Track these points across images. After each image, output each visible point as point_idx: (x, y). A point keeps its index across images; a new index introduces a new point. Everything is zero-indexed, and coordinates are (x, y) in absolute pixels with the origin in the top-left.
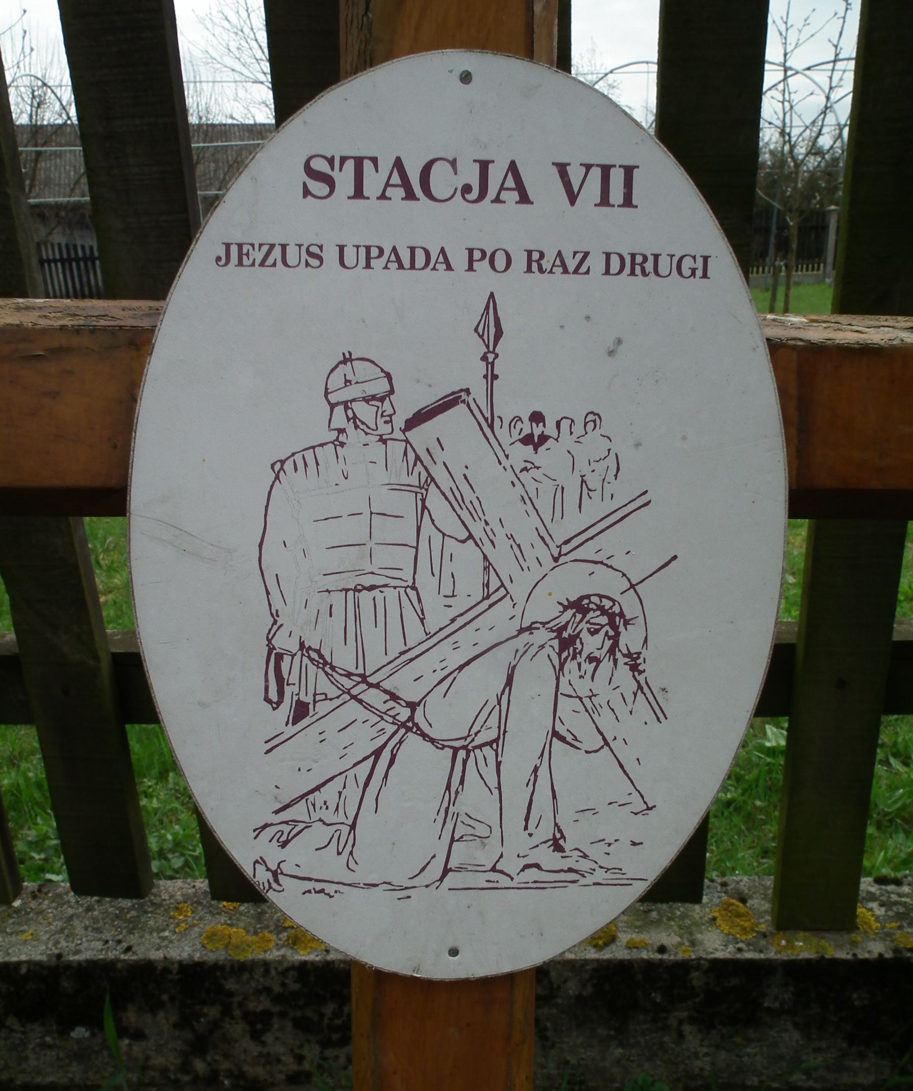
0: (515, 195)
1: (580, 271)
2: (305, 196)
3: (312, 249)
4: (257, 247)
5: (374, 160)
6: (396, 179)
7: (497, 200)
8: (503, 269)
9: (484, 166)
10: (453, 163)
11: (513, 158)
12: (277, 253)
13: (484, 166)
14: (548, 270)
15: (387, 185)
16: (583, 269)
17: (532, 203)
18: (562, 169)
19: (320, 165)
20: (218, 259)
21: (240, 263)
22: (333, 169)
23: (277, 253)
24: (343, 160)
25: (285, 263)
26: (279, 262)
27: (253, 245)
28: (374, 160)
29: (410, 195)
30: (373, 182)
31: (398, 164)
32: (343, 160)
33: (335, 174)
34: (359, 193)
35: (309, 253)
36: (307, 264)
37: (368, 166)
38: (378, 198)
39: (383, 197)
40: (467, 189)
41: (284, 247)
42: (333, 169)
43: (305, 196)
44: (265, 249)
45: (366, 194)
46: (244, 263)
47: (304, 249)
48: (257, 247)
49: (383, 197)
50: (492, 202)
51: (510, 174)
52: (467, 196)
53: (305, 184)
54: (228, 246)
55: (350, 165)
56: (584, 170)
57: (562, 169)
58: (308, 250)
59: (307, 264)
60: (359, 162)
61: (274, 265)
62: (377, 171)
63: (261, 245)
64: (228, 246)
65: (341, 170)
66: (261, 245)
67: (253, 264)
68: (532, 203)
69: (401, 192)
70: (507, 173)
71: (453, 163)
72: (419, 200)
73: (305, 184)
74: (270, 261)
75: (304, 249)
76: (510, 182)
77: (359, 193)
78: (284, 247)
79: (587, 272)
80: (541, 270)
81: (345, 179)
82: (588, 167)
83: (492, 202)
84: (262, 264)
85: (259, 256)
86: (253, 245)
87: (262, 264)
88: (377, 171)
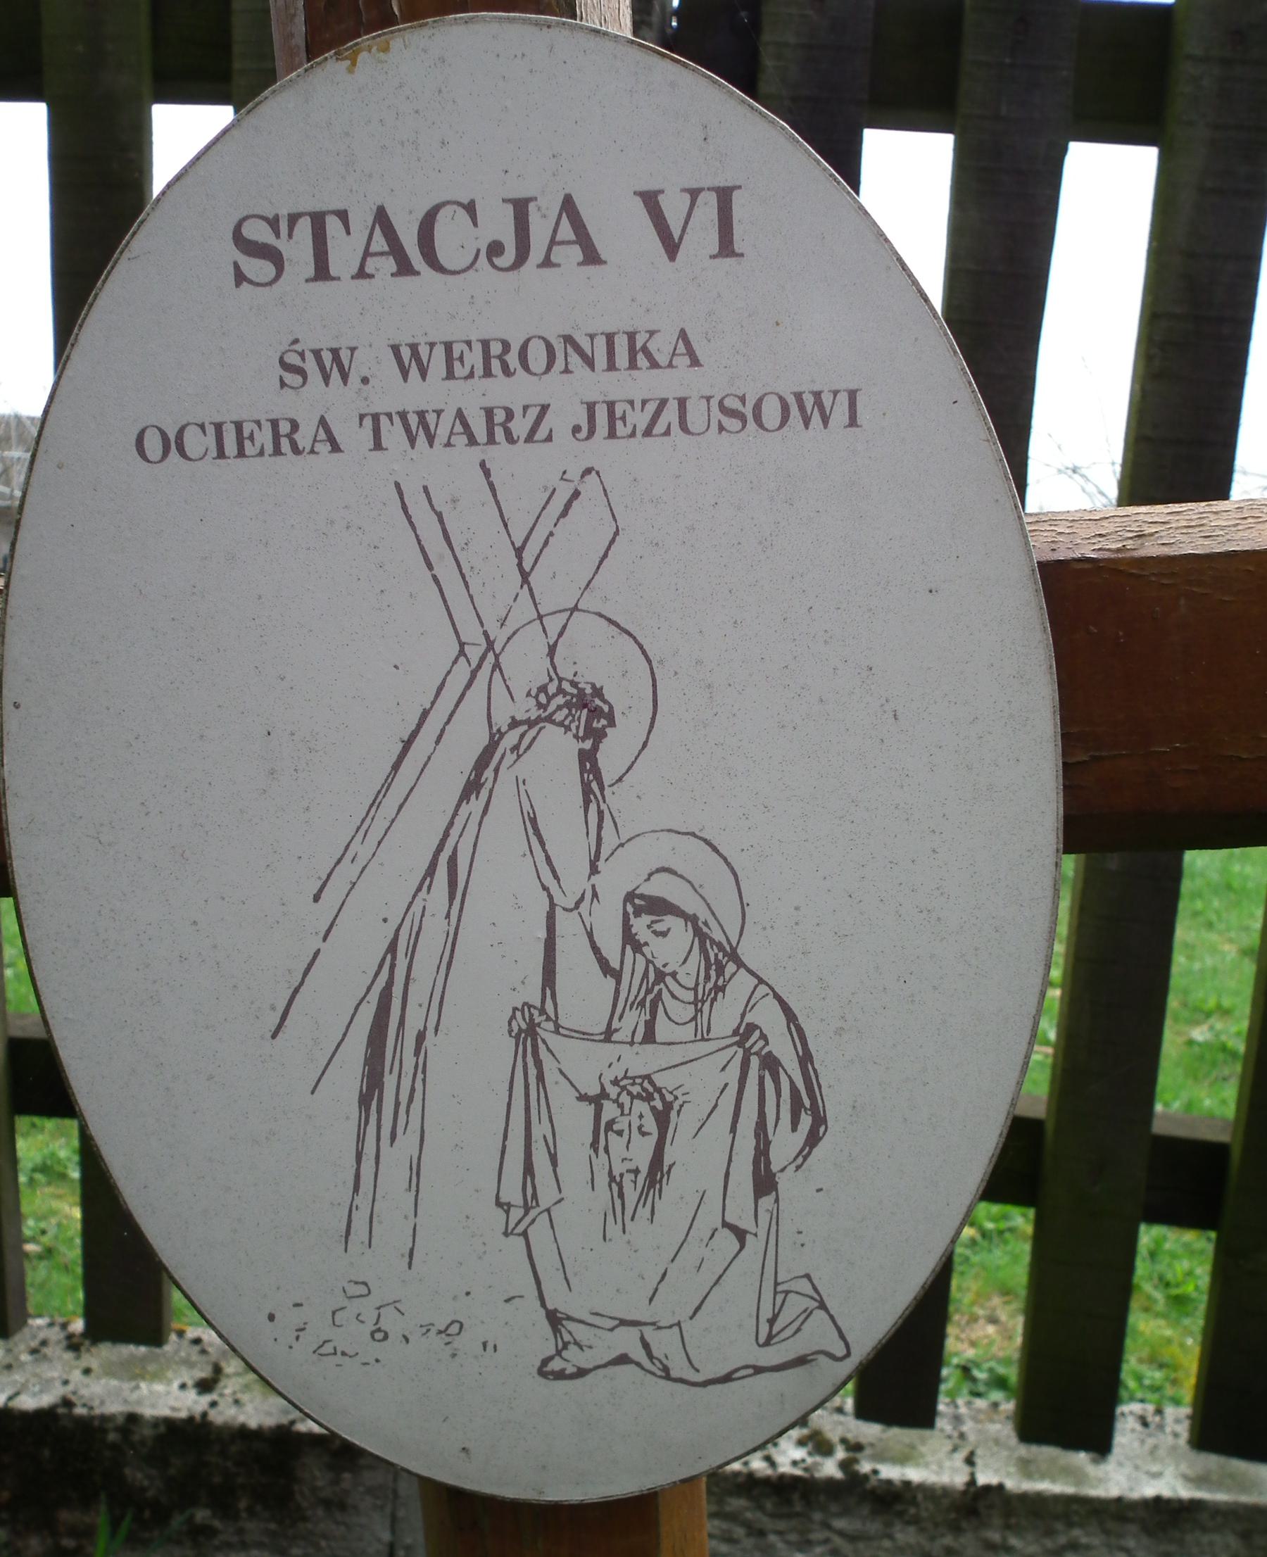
0: (576, 253)
1: (654, 432)
2: (238, 284)
3: (729, 403)
4: (638, 405)
5: (343, 215)
6: (380, 243)
7: (547, 263)
8: (159, 458)
9: (521, 208)
10: (470, 208)
11: (567, 191)
12: (670, 415)
13: (521, 208)
14: (308, 449)
15: (367, 254)
16: (542, 433)
17: (605, 262)
18: (651, 200)
19: (257, 232)
20: (576, 429)
21: (612, 434)
22: (278, 235)
23: (670, 415)
24: (293, 219)
25: (684, 427)
26: (675, 428)
27: (631, 403)
28: (343, 215)
29: (405, 268)
30: (344, 251)
31: (381, 218)
32: (293, 219)
33: (282, 245)
34: (322, 272)
35: (723, 409)
36: (721, 428)
37: (333, 224)
38: (353, 278)
39: (362, 274)
40: (495, 249)
41: (682, 403)
42: (278, 235)
43: (238, 284)
44: (651, 407)
45: (333, 272)
46: (618, 434)
47: (714, 403)
48: (638, 405)
49: (362, 274)
50: (539, 266)
51: (676, 236)
52: (497, 261)
53: (236, 266)
54: (591, 408)
55: (304, 226)
56: (687, 197)
57: (651, 200)
58: (721, 403)
59: (721, 428)
60: (318, 221)
61: (667, 432)
62: (348, 233)
63: (644, 403)
64: (591, 408)
65: (290, 236)
66: (644, 403)
67: (633, 434)
68: (605, 262)
69: (390, 264)
70: (681, 238)
71: (470, 208)
72: (418, 273)
73: (236, 266)
74: (660, 428)
75: (714, 403)
76: (566, 231)
77: (322, 272)
78: (682, 403)
79: (549, 438)
80: (296, 450)
81: (298, 250)
82: (694, 193)
83: (539, 266)
84: (648, 433)
85: (640, 419)
86: (631, 403)
87: (648, 433)
88: (348, 233)
